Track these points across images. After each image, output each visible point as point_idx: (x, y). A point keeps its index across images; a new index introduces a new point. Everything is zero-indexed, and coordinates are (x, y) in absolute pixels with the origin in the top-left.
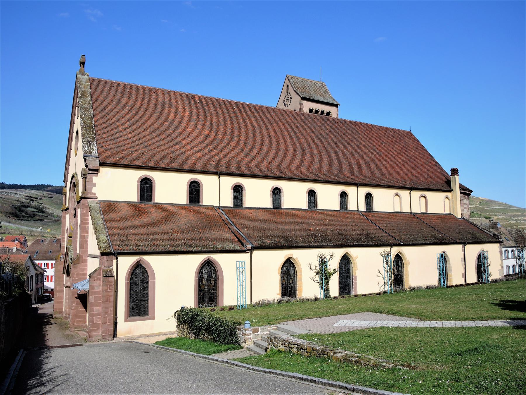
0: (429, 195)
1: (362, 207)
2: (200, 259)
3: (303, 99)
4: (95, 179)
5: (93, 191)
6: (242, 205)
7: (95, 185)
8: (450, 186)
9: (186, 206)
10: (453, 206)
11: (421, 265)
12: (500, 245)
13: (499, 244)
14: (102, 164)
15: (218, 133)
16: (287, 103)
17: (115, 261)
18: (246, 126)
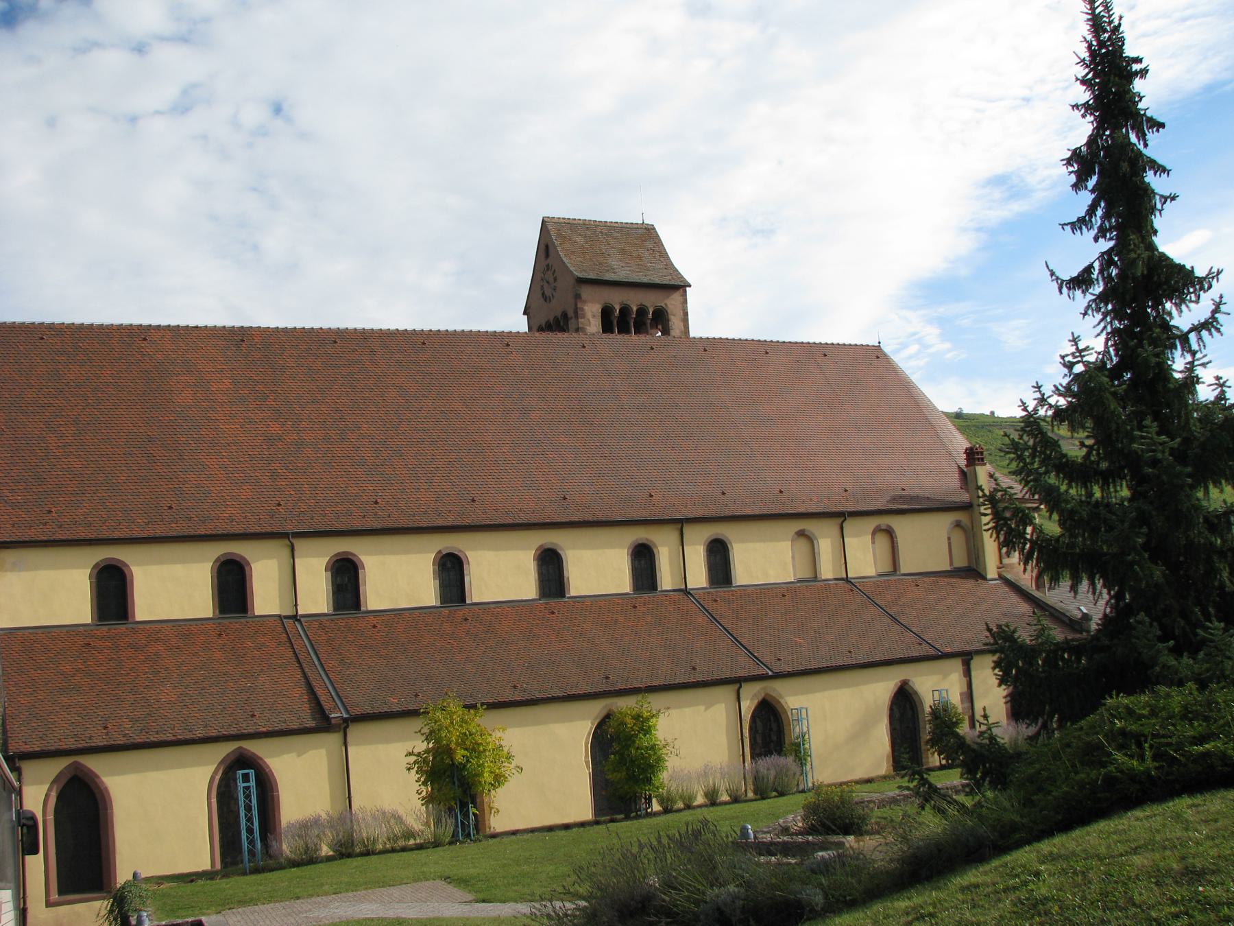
16: (548, 292)
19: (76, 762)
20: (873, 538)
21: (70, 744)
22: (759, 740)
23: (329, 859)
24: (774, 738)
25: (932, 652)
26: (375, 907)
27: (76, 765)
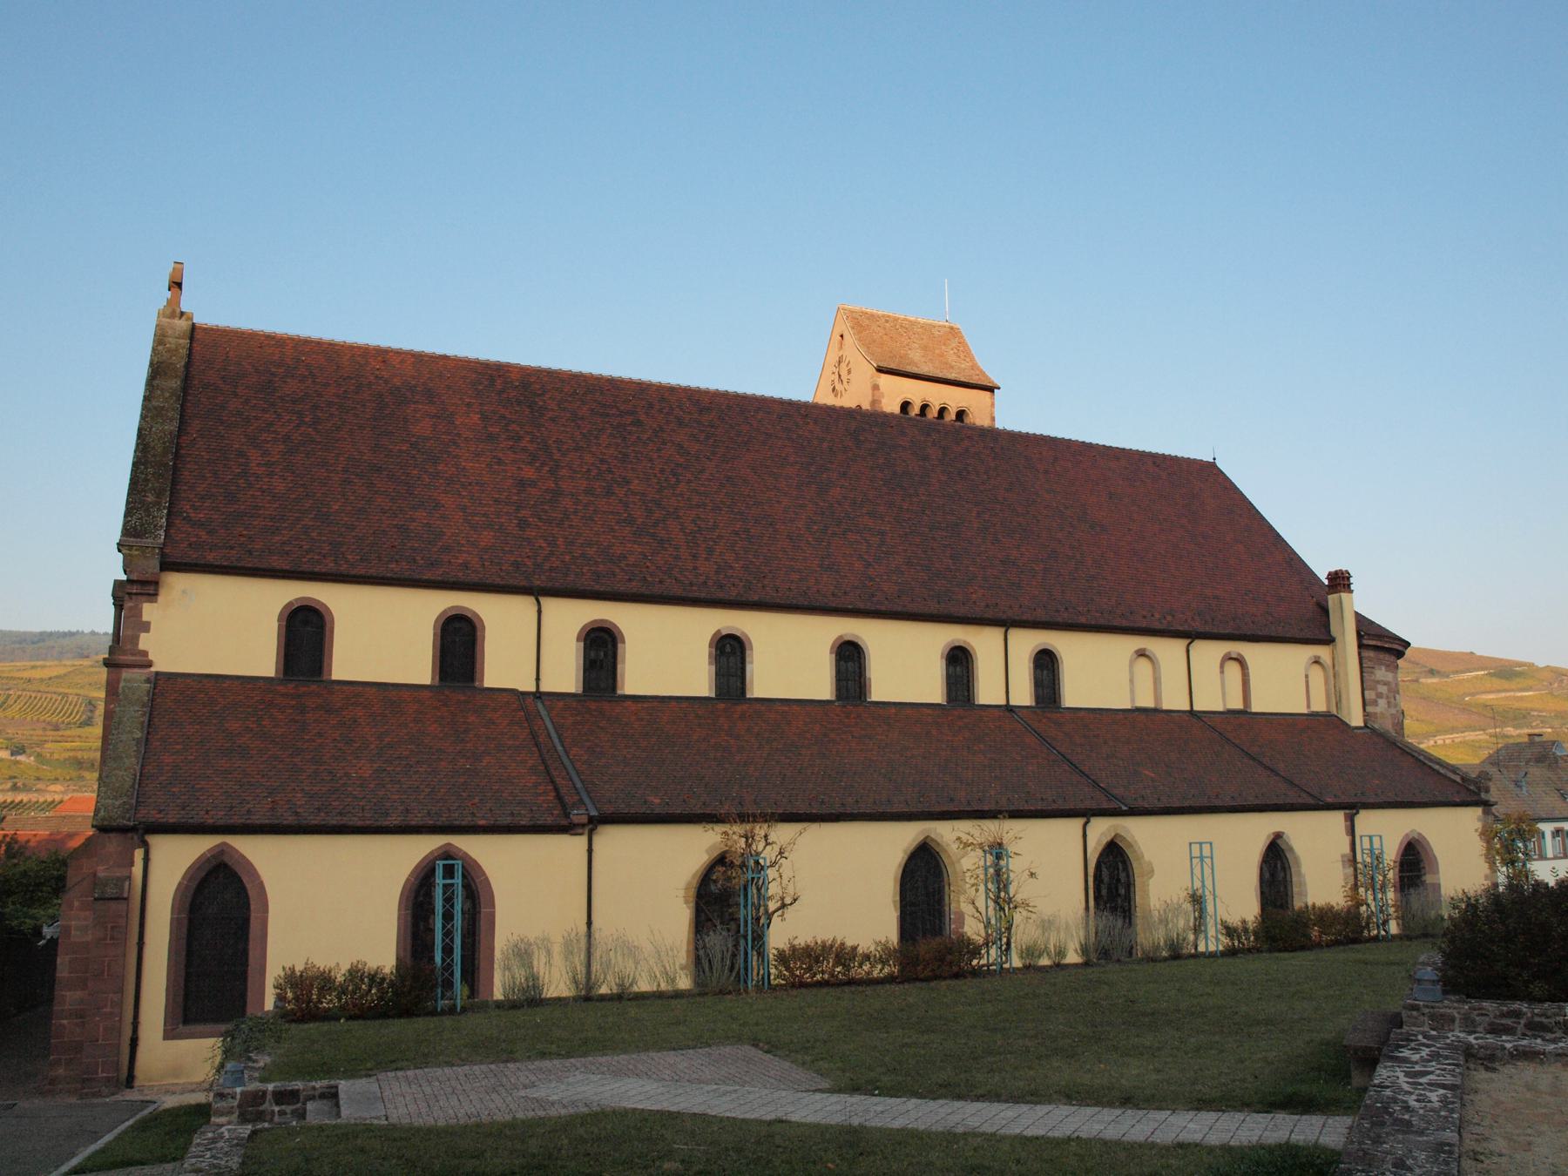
0: (1254, 653)
1: (1023, 695)
2: (413, 851)
3: (880, 370)
4: (149, 611)
5: (141, 646)
6: (614, 687)
7: (146, 627)
8: (1326, 625)
9: (427, 694)
10: (1336, 693)
11: (1200, 868)
12: (1486, 813)
13: (1479, 811)
14: (169, 565)
15: (563, 472)
16: (839, 387)
17: (139, 854)
18: (659, 450)
19: (225, 844)
20: (1222, 666)
21: (218, 817)
22: (1104, 892)
23: (1165, 959)
24: (1122, 891)
25: (1311, 801)
26: (651, 1087)
27: (222, 850)
